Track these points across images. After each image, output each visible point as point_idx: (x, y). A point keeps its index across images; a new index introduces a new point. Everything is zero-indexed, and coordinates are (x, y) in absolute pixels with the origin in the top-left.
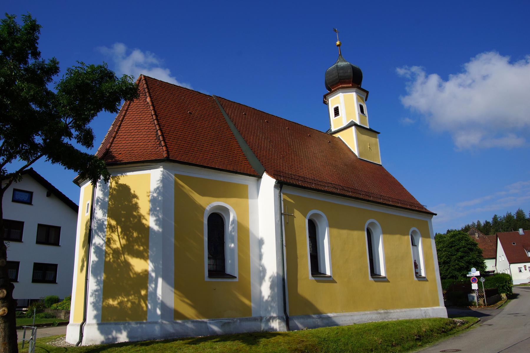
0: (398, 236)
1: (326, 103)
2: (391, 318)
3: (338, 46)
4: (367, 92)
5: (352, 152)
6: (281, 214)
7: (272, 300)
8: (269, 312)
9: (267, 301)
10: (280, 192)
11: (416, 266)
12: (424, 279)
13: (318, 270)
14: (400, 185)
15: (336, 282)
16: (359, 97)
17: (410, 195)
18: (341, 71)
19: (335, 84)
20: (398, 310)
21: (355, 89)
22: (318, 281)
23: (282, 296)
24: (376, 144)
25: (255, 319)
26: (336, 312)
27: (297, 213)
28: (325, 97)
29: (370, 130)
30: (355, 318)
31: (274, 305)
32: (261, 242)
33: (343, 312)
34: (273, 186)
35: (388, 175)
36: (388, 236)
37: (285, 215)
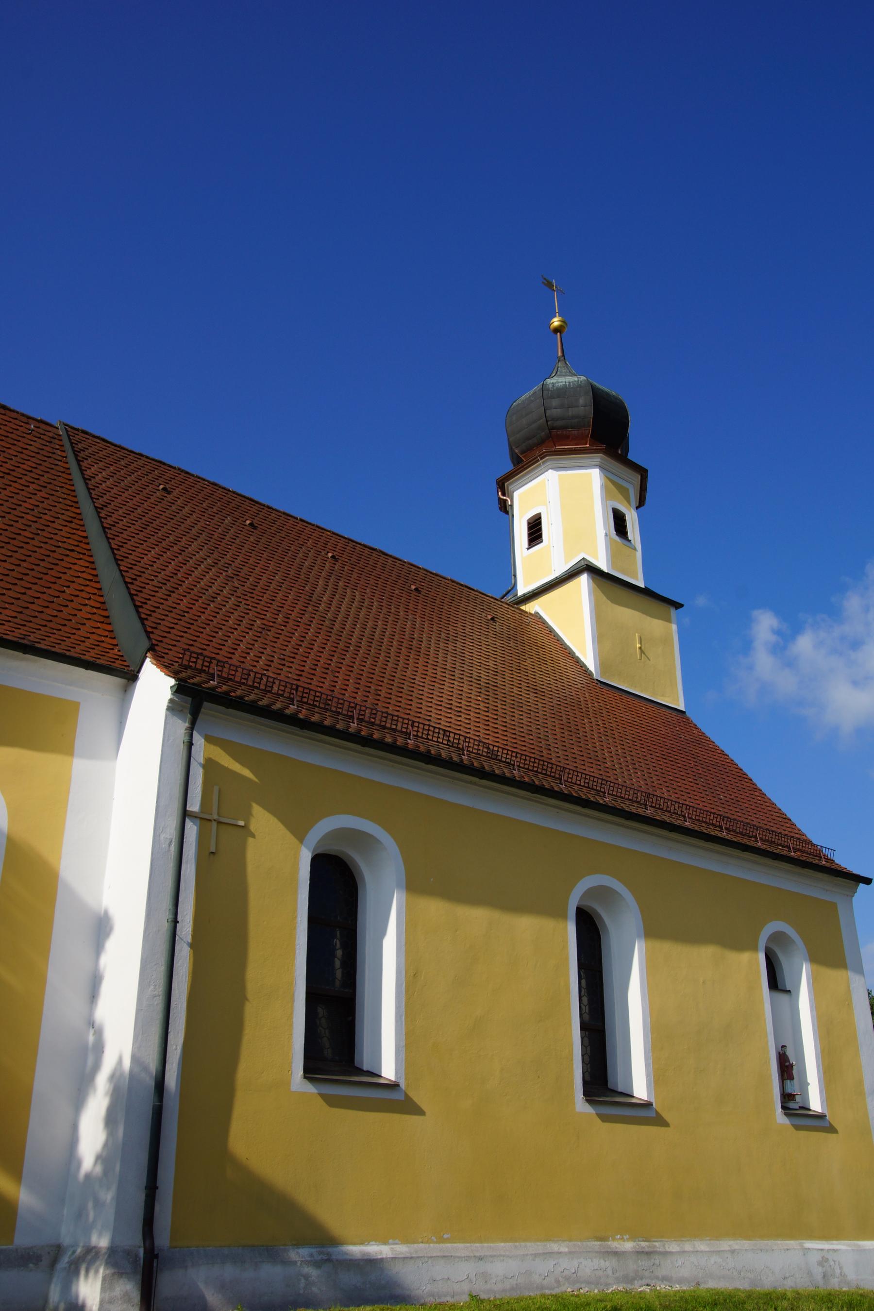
0: (708, 952)
1: (505, 508)
2: (664, 1279)
3: (557, 330)
4: (643, 472)
5: (577, 661)
6: (185, 814)
7: (106, 1172)
8: (88, 1230)
9: (88, 1176)
10: (191, 729)
11: (786, 1068)
12: (818, 1123)
13: (607, 1084)
14: (742, 776)
15: (420, 1112)
16: (612, 484)
17: (715, 750)
18: (555, 402)
19: (540, 442)
20: (702, 1246)
21: (598, 458)
22: (331, 1101)
23: (142, 1157)
24: (666, 641)
25: (27, 1258)
26: (406, 1241)
27: (264, 824)
28: (503, 485)
29: (646, 592)
30: (498, 1269)
31: (108, 1196)
32: (101, 928)
33: (441, 1240)
34: (166, 707)
35: (701, 741)
36: (666, 947)
37: (202, 819)
